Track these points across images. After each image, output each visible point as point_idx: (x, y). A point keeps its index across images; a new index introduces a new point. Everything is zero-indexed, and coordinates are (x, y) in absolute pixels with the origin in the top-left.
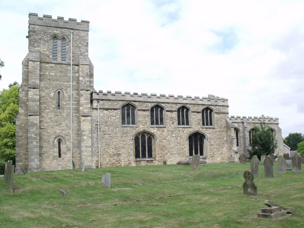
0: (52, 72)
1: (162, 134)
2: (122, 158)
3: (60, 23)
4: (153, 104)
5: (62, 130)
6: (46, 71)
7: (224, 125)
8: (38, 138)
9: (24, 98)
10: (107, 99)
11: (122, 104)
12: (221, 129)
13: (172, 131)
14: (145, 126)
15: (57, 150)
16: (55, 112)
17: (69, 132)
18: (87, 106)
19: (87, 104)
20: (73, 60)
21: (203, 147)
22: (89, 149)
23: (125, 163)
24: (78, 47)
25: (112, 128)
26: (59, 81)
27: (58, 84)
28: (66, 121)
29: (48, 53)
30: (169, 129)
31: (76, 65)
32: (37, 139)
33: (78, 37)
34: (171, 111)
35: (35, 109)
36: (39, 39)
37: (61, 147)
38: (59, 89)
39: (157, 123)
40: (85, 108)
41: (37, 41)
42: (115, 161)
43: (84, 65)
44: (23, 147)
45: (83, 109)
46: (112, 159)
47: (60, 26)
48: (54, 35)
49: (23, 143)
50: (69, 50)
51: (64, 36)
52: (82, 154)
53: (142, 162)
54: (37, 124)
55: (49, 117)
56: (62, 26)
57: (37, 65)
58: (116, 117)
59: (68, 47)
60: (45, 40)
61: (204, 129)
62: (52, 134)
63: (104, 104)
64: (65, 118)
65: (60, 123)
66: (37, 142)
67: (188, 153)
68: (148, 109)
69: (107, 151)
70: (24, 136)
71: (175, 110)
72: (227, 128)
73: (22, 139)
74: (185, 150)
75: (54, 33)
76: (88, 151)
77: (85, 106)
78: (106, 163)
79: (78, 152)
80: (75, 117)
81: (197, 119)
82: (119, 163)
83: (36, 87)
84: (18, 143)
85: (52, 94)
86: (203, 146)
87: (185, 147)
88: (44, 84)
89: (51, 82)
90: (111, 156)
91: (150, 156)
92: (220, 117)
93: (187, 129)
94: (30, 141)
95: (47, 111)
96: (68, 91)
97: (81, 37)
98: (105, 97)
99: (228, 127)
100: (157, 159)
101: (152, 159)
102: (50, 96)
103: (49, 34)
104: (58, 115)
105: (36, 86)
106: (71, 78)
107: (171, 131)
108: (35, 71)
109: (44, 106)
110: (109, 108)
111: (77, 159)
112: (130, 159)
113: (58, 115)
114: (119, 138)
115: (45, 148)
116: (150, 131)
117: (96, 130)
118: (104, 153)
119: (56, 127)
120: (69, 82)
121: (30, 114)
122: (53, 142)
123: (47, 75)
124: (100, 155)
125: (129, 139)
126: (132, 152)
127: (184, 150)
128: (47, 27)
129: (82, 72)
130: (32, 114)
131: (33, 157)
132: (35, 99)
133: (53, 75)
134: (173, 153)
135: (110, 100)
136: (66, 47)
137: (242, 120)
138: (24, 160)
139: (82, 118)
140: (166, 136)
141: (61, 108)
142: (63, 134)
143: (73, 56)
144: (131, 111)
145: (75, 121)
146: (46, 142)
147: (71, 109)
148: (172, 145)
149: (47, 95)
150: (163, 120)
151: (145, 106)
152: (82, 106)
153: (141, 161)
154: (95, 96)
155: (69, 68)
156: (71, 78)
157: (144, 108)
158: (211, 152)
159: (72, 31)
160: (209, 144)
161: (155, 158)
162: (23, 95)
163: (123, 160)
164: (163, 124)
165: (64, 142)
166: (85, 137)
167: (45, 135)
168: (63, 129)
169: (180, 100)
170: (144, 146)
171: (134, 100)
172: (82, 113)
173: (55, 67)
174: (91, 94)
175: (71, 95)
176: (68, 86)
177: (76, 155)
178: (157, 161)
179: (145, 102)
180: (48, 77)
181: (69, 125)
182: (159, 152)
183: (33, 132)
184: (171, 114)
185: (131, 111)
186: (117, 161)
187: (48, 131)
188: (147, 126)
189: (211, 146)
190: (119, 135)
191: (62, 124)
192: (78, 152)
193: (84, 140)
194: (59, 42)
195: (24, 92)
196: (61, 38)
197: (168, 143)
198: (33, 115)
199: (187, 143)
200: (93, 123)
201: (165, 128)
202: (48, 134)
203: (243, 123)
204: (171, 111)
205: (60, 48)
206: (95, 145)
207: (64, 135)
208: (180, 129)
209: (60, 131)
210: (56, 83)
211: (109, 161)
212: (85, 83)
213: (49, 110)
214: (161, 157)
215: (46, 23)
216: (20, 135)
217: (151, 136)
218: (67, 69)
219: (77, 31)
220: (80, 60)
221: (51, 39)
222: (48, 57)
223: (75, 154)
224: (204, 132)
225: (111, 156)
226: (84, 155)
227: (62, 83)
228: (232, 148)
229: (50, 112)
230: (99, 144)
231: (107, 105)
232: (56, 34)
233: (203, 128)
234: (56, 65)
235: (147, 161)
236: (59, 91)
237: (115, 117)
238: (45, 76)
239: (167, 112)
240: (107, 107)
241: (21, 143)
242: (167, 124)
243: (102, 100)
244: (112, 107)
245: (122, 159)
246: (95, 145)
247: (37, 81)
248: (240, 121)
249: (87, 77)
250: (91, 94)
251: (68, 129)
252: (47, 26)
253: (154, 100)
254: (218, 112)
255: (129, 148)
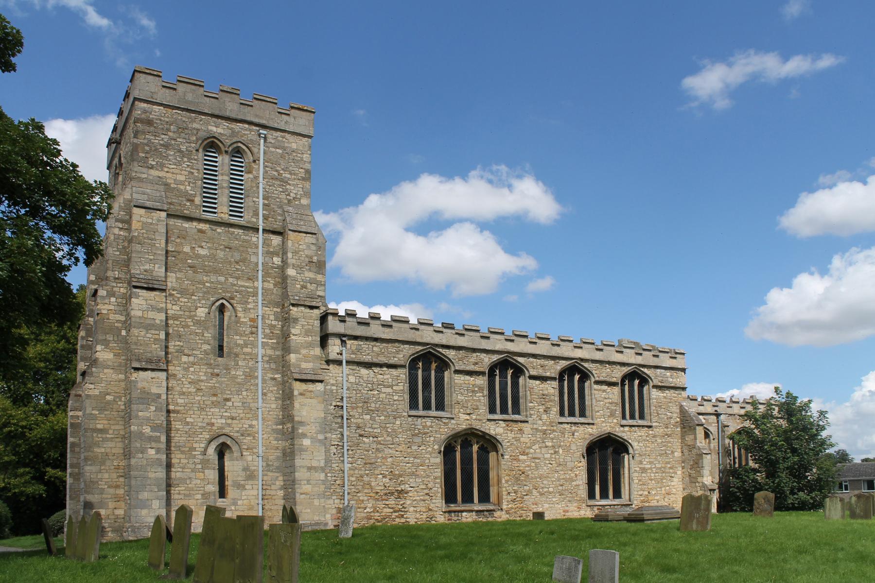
0: (202, 247)
1: (517, 440)
2: (408, 502)
3: (228, 104)
4: (495, 358)
5: (233, 419)
6: (183, 241)
7: (676, 418)
8: (163, 439)
9: (112, 316)
10: (368, 334)
11: (411, 352)
12: (667, 428)
13: (544, 432)
14: (474, 417)
15: (212, 475)
16: (209, 365)
17: (250, 426)
18: (312, 353)
19: (310, 345)
20: (265, 218)
21: (622, 477)
22: (316, 474)
23: (418, 515)
24: (282, 180)
25: (382, 418)
26: (222, 275)
27: (220, 283)
28: (244, 393)
29: (188, 188)
30: (535, 426)
31: (274, 232)
32: (160, 442)
33: (280, 151)
34: (543, 379)
35: (151, 352)
36: (161, 145)
37: (226, 469)
38: (222, 298)
39: (504, 411)
40: (305, 356)
41: (156, 150)
42: (392, 510)
43: (300, 232)
44: (108, 463)
45: (298, 360)
46: (381, 505)
47: (228, 114)
48: (208, 138)
49: (108, 450)
50: (252, 187)
51: (240, 145)
52: (298, 490)
53: (464, 514)
54: (159, 396)
55: (192, 377)
56: (233, 116)
57: (159, 220)
58: (394, 388)
59: (251, 176)
60: (180, 151)
61: (627, 429)
62: (201, 427)
63: (359, 350)
64: (239, 384)
65: (225, 396)
66: (158, 451)
67: (583, 492)
68: (482, 370)
69: (369, 484)
70: (111, 432)
71: (553, 375)
72: (684, 428)
73: (105, 440)
74: (578, 483)
75: (208, 131)
76: (314, 482)
77: (304, 351)
78: (365, 515)
79: (277, 483)
80: (270, 383)
81: (608, 401)
82: (402, 516)
83: (155, 286)
84: (93, 452)
85: (201, 312)
86: (622, 473)
87: (576, 475)
88: (177, 278)
89: (199, 277)
90: (378, 497)
91: (485, 497)
92: (665, 397)
93: (582, 428)
94: (138, 445)
95: (185, 359)
96: (249, 306)
97: (288, 150)
98: (362, 332)
99: (687, 424)
100: (504, 507)
101: (491, 508)
102: (196, 316)
103: (193, 134)
104: (218, 375)
105: (155, 282)
106: (260, 267)
107: (540, 431)
108: (152, 240)
109: (175, 346)
110: (375, 360)
111: (277, 502)
112: (432, 505)
113: (218, 375)
114: (400, 448)
115: (180, 470)
116: (487, 431)
117: (336, 423)
118: (360, 487)
119: (212, 410)
120: (252, 278)
121: (137, 365)
122: (204, 453)
123: (187, 253)
124: (348, 494)
125: (430, 449)
126: (438, 488)
127: (574, 483)
128: (188, 114)
129: (295, 253)
130: (144, 365)
131: (144, 495)
132: (152, 322)
133: (204, 256)
134: (546, 490)
135: (376, 340)
136: (242, 176)
137: (716, 408)
138: (110, 503)
139: (298, 387)
140: (528, 445)
141: (229, 353)
142: (234, 429)
143: (264, 205)
144: (433, 373)
145: (269, 395)
146: (183, 452)
147: (260, 359)
148: (544, 470)
149: (187, 313)
150: (521, 401)
151: (472, 360)
152: (297, 352)
153: (462, 511)
154: (333, 325)
155: (254, 239)
156: (260, 267)
157: (471, 368)
158: (641, 490)
159: (265, 132)
160: (638, 469)
161: (499, 503)
162: (112, 307)
163: (412, 509)
164: (519, 413)
165: (236, 454)
166: (306, 442)
167: (178, 430)
168: (233, 415)
169: (564, 348)
170: (468, 464)
171: (444, 342)
172: (297, 370)
173: (209, 233)
174: (323, 319)
175: (260, 318)
176: (250, 292)
177: (272, 493)
178: (504, 512)
179: (474, 350)
180: (189, 261)
181: (252, 405)
182: (510, 489)
183: (148, 419)
184: (543, 385)
185: (433, 373)
186: (395, 512)
187: (188, 420)
188: (478, 417)
189: (644, 475)
190: (402, 438)
191: (233, 400)
192: (277, 483)
193: (302, 450)
194: (223, 161)
195: (113, 299)
196: (230, 149)
197: (533, 464)
198: (145, 370)
199: (584, 463)
200: (329, 403)
201: (526, 424)
202: (187, 428)
203: (718, 415)
204: (543, 379)
205: (227, 178)
206: (334, 465)
207: (238, 432)
208: (566, 426)
209: (224, 421)
210: (213, 278)
211: (373, 512)
212: (303, 287)
213: (191, 359)
214: (514, 501)
215: (187, 102)
216: (99, 426)
217: (489, 444)
218: (245, 241)
219: (279, 134)
220: (288, 219)
221: (201, 150)
222: (188, 200)
223: (269, 487)
224: (625, 438)
225: (378, 497)
226: (302, 491)
227: (231, 280)
228: (699, 479)
229: (194, 364)
230: (346, 461)
231: (369, 352)
232: (216, 135)
233: (622, 426)
234: (214, 227)
235: (477, 511)
236: (222, 304)
237: (391, 386)
238: (181, 256)
239: (531, 381)
240: (367, 359)
241: (103, 450)
242: (532, 412)
243: (356, 338)
244: (382, 359)
245: (411, 505)
246: (334, 465)
247: (159, 268)
248: (708, 408)
249: (310, 270)
250: (323, 319)
251: (250, 416)
252: (188, 110)
253: (498, 347)
254: (660, 384)
255: (428, 476)
